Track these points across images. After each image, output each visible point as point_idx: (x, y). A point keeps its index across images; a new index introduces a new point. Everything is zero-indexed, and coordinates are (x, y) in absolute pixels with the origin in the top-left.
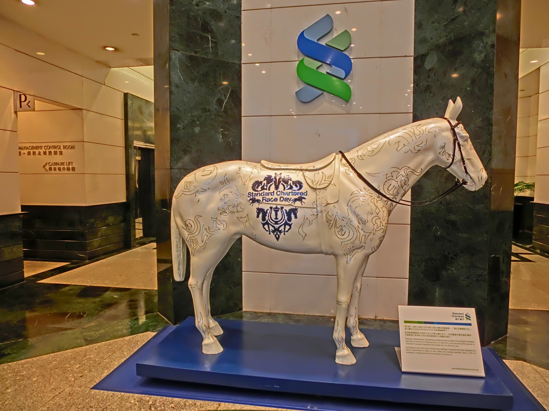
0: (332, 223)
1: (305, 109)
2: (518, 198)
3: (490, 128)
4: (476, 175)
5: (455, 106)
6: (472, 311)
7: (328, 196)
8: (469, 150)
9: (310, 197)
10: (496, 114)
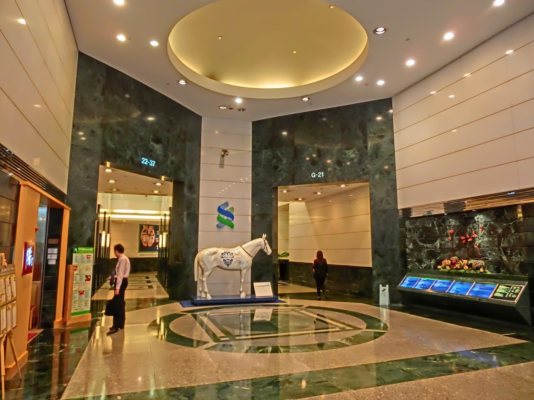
0: (240, 262)
1: (220, 229)
2: (280, 260)
3: (272, 240)
4: (269, 251)
5: (264, 236)
6: (269, 283)
7: (239, 257)
8: (268, 246)
9: (235, 257)
10: (273, 235)
